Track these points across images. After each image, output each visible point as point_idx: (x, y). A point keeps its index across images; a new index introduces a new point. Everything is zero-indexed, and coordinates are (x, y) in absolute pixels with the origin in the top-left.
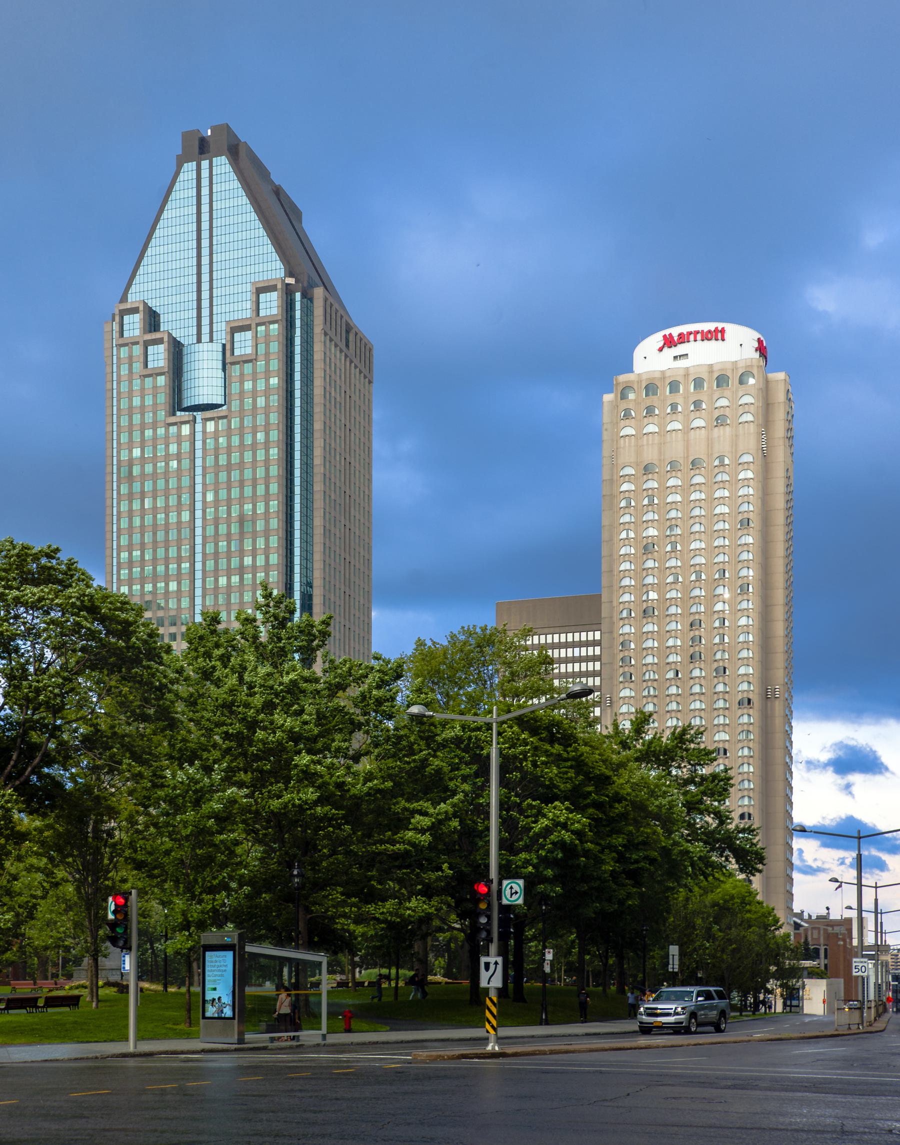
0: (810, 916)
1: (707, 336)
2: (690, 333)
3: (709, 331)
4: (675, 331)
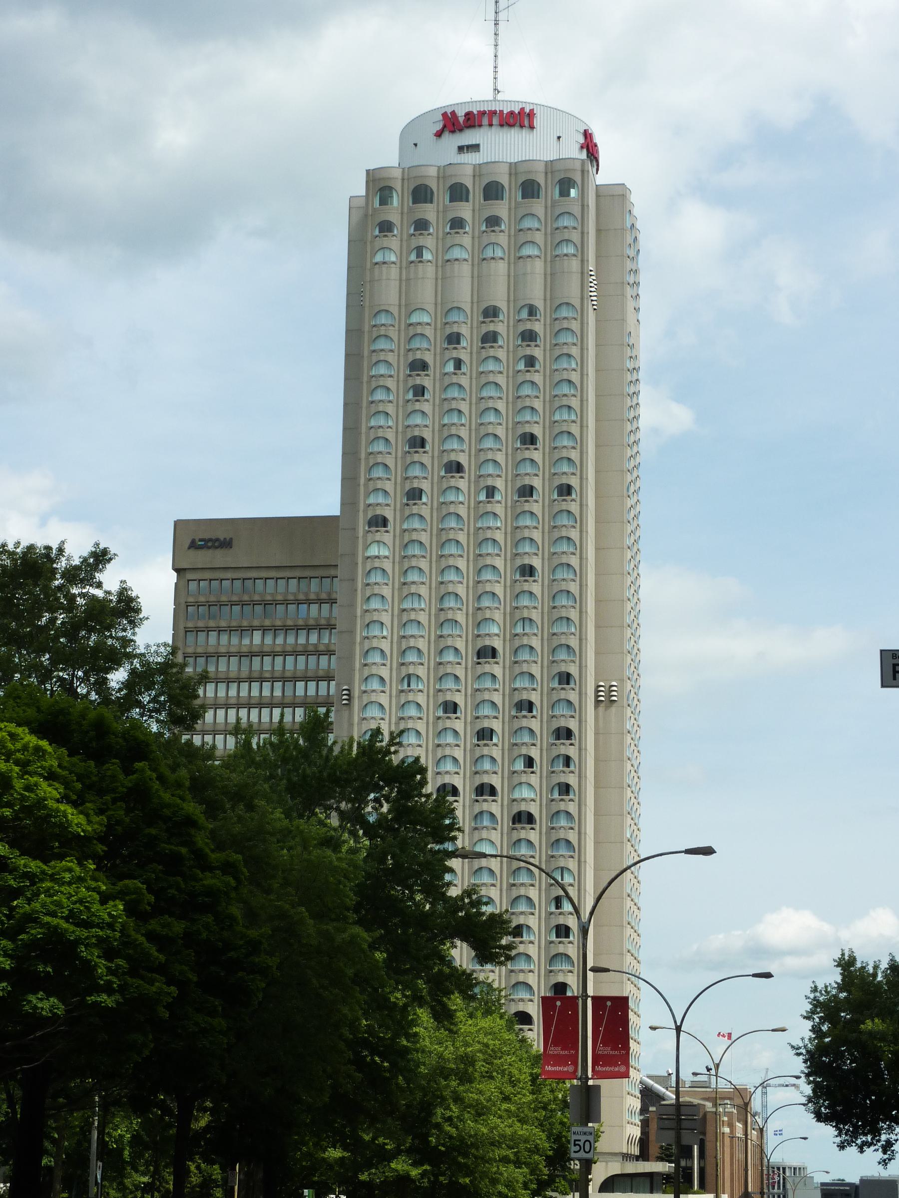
0: (836, 983)
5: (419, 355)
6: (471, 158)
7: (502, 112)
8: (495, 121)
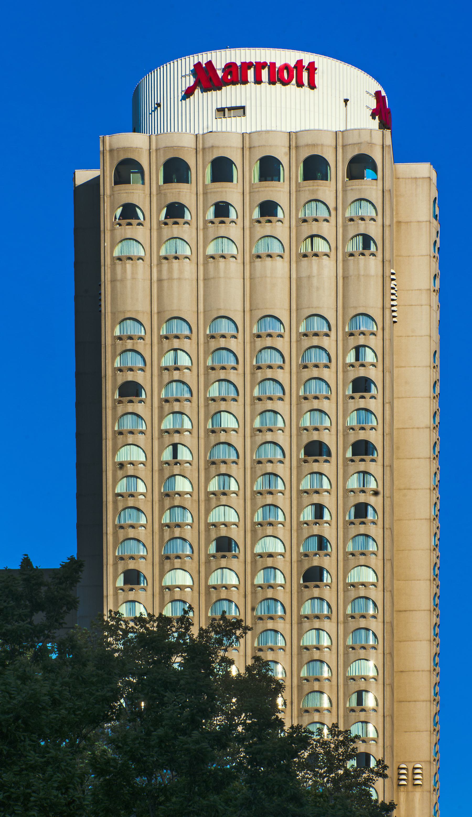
1: (279, 76)
2: (246, 66)
3: (286, 67)
4: (220, 59)
5: (130, 376)
6: (234, 125)
7: (273, 64)
8: (265, 73)
